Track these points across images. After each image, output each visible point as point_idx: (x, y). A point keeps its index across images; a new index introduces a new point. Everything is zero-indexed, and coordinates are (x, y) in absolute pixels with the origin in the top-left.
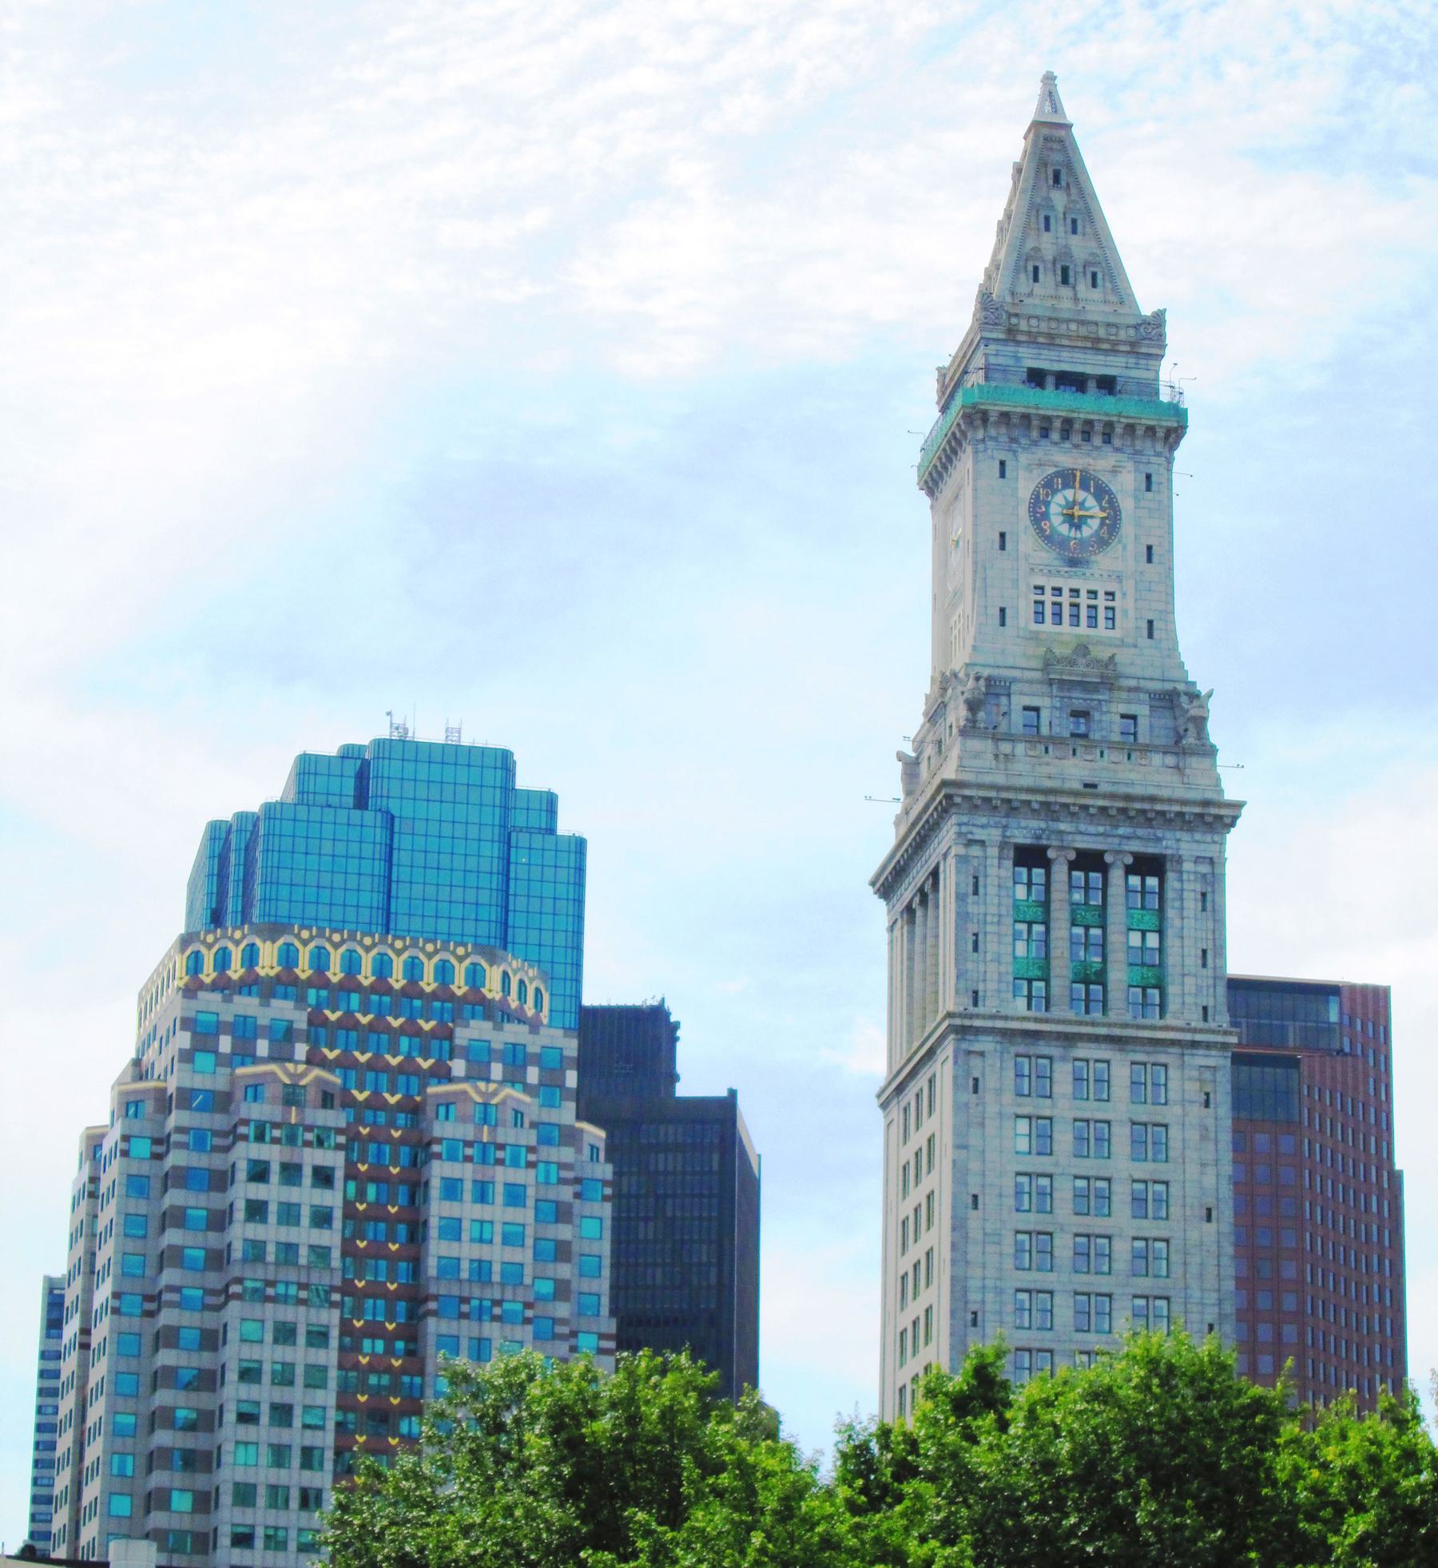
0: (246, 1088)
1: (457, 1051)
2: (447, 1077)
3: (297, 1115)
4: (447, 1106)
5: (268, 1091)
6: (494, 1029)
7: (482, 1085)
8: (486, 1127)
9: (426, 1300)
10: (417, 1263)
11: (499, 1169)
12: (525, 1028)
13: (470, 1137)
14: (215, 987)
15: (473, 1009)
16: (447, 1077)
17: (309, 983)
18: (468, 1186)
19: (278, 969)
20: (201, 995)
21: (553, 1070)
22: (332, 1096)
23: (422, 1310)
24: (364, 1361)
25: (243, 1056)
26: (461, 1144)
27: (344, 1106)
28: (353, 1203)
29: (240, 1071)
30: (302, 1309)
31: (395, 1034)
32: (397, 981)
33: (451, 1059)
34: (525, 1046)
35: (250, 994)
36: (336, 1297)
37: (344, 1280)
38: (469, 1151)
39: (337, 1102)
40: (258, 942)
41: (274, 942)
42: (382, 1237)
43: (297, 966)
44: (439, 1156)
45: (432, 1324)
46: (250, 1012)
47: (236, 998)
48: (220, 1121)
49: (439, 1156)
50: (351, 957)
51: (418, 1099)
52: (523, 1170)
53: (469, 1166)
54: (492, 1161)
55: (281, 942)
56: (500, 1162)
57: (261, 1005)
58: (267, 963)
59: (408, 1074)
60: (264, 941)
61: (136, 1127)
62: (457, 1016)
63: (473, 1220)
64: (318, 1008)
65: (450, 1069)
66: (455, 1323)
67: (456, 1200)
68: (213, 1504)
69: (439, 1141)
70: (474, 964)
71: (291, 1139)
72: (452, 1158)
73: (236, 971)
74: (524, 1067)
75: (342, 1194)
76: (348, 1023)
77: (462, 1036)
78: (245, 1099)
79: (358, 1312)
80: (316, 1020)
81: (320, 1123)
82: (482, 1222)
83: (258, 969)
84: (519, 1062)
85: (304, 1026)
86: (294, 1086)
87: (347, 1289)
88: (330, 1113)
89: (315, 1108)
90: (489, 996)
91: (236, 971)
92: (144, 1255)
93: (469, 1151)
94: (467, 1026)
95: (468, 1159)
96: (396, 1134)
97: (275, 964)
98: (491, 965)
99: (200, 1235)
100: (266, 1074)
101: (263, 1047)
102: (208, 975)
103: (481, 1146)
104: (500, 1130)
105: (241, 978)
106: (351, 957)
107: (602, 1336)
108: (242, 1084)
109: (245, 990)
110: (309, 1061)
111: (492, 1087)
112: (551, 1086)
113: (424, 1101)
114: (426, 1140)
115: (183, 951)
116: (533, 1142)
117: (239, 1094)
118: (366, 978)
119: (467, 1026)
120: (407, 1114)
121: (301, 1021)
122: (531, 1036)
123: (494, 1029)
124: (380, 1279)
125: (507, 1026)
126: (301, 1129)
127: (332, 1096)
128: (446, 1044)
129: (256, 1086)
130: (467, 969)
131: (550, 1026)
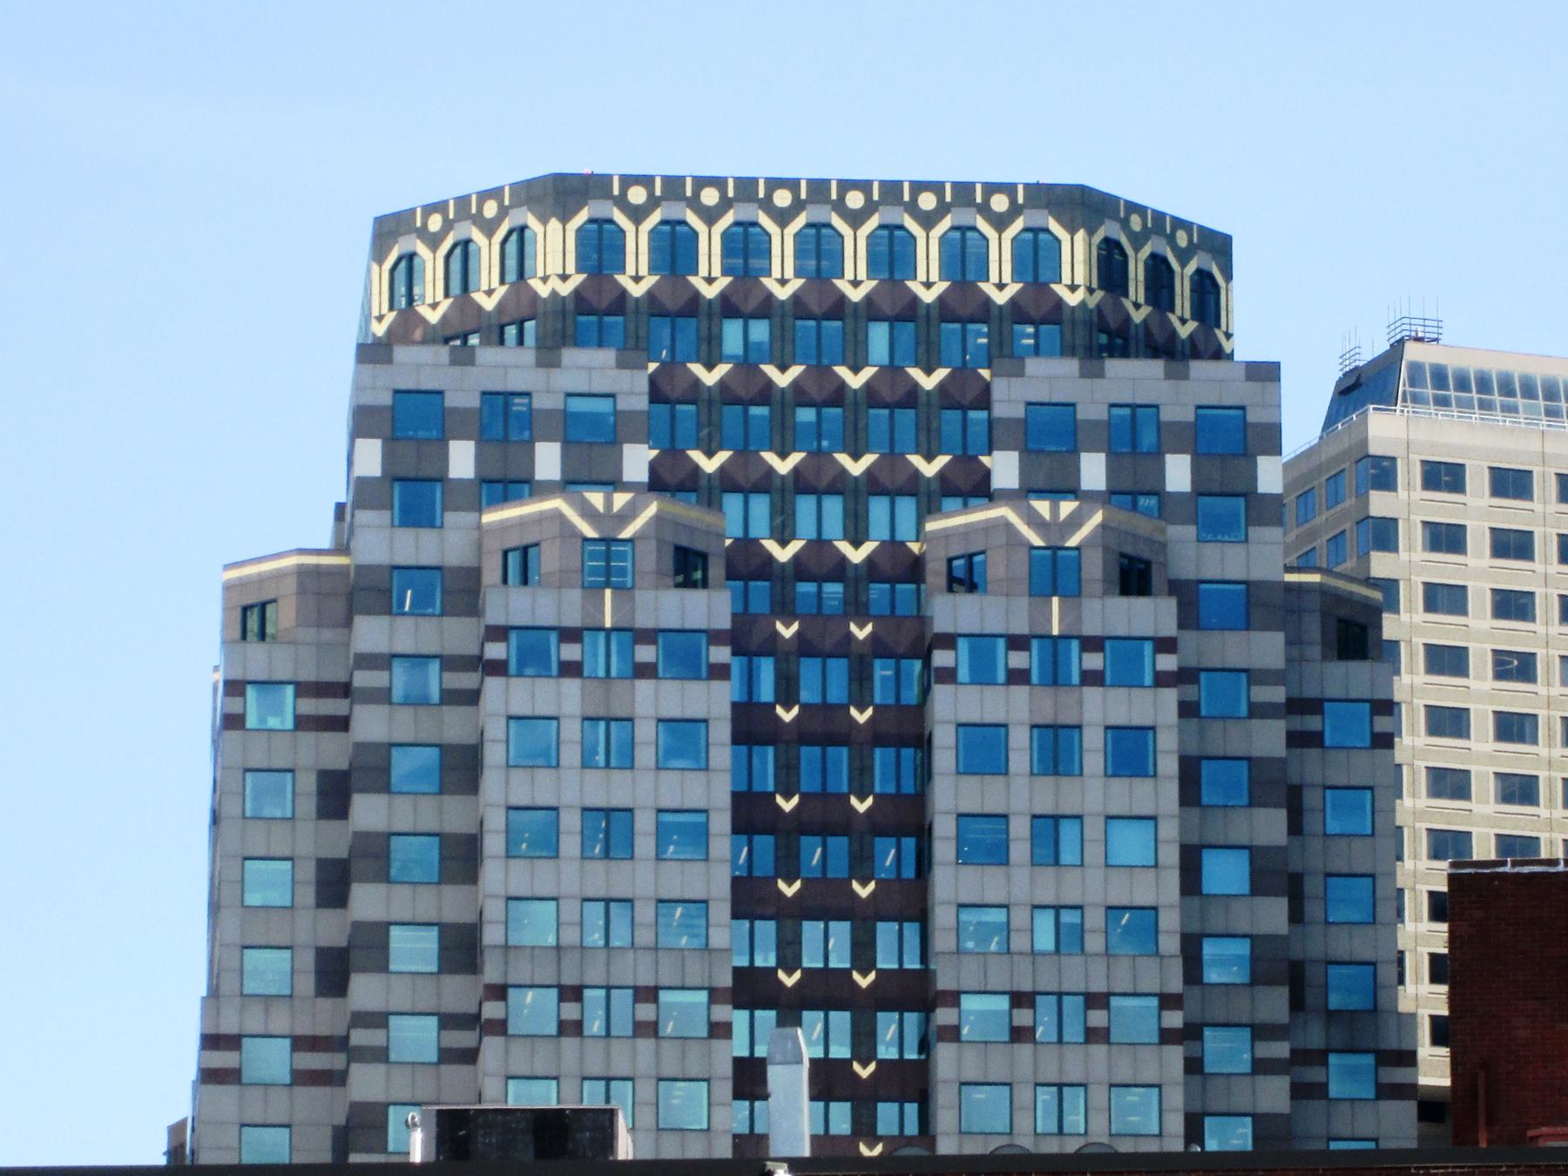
0: (505, 553)
2: (979, 488)
5: (549, 560)
7: (596, 498)
12: (1157, 367)
13: (1020, 627)
14: (444, 335)
16: (979, 488)
18: (1020, 740)
19: (577, 280)
29: (490, 518)
31: (783, 403)
38: (1018, 660)
41: (564, 220)
42: (838, 869)
43: (622, 270)
46: (515, 383)
48: (459, 635)
49: (949, 675)
51: (915, 547)
53: (1020, 693)
54: (1076, 679)
55: (582, 217)
56: (1092, 678)
57: (1084, 374)
58: (555, 267)
59: (893, 493)
60: (544, 221)
61: (258, 660)
62: (1003, 354)
65: (987, 474)
67: (1069, 774)
71: (1055, 677)
72: (982, 676)
74: (1158, 455)
77: (1009, 399)
78: (505, 581)
83: (535, 283)
84: (1148, 440)
85: (641, 403)
86: (608, 541)
88: (696, 597)
93: (1018, 660)
94: (1020, 373)
95: (1018, 677)
97: (571, 269)
99: (427, 895)
100: (541, 518)
101: (548, 460)
102: (434, 306)
107: (380, 1055)
108: (494, 547)
110: (657, 484)
111: (621, 499)
116: (1169, 627)
117: (491, 575)
118: (856, 283)
119: (1020, 373)
121: (632, 388)
122: (542, 372)
124: (759, 962)
125: (1116, 367)
126: (1075, 645)
129: (525, 550)
131: (1036, 351)
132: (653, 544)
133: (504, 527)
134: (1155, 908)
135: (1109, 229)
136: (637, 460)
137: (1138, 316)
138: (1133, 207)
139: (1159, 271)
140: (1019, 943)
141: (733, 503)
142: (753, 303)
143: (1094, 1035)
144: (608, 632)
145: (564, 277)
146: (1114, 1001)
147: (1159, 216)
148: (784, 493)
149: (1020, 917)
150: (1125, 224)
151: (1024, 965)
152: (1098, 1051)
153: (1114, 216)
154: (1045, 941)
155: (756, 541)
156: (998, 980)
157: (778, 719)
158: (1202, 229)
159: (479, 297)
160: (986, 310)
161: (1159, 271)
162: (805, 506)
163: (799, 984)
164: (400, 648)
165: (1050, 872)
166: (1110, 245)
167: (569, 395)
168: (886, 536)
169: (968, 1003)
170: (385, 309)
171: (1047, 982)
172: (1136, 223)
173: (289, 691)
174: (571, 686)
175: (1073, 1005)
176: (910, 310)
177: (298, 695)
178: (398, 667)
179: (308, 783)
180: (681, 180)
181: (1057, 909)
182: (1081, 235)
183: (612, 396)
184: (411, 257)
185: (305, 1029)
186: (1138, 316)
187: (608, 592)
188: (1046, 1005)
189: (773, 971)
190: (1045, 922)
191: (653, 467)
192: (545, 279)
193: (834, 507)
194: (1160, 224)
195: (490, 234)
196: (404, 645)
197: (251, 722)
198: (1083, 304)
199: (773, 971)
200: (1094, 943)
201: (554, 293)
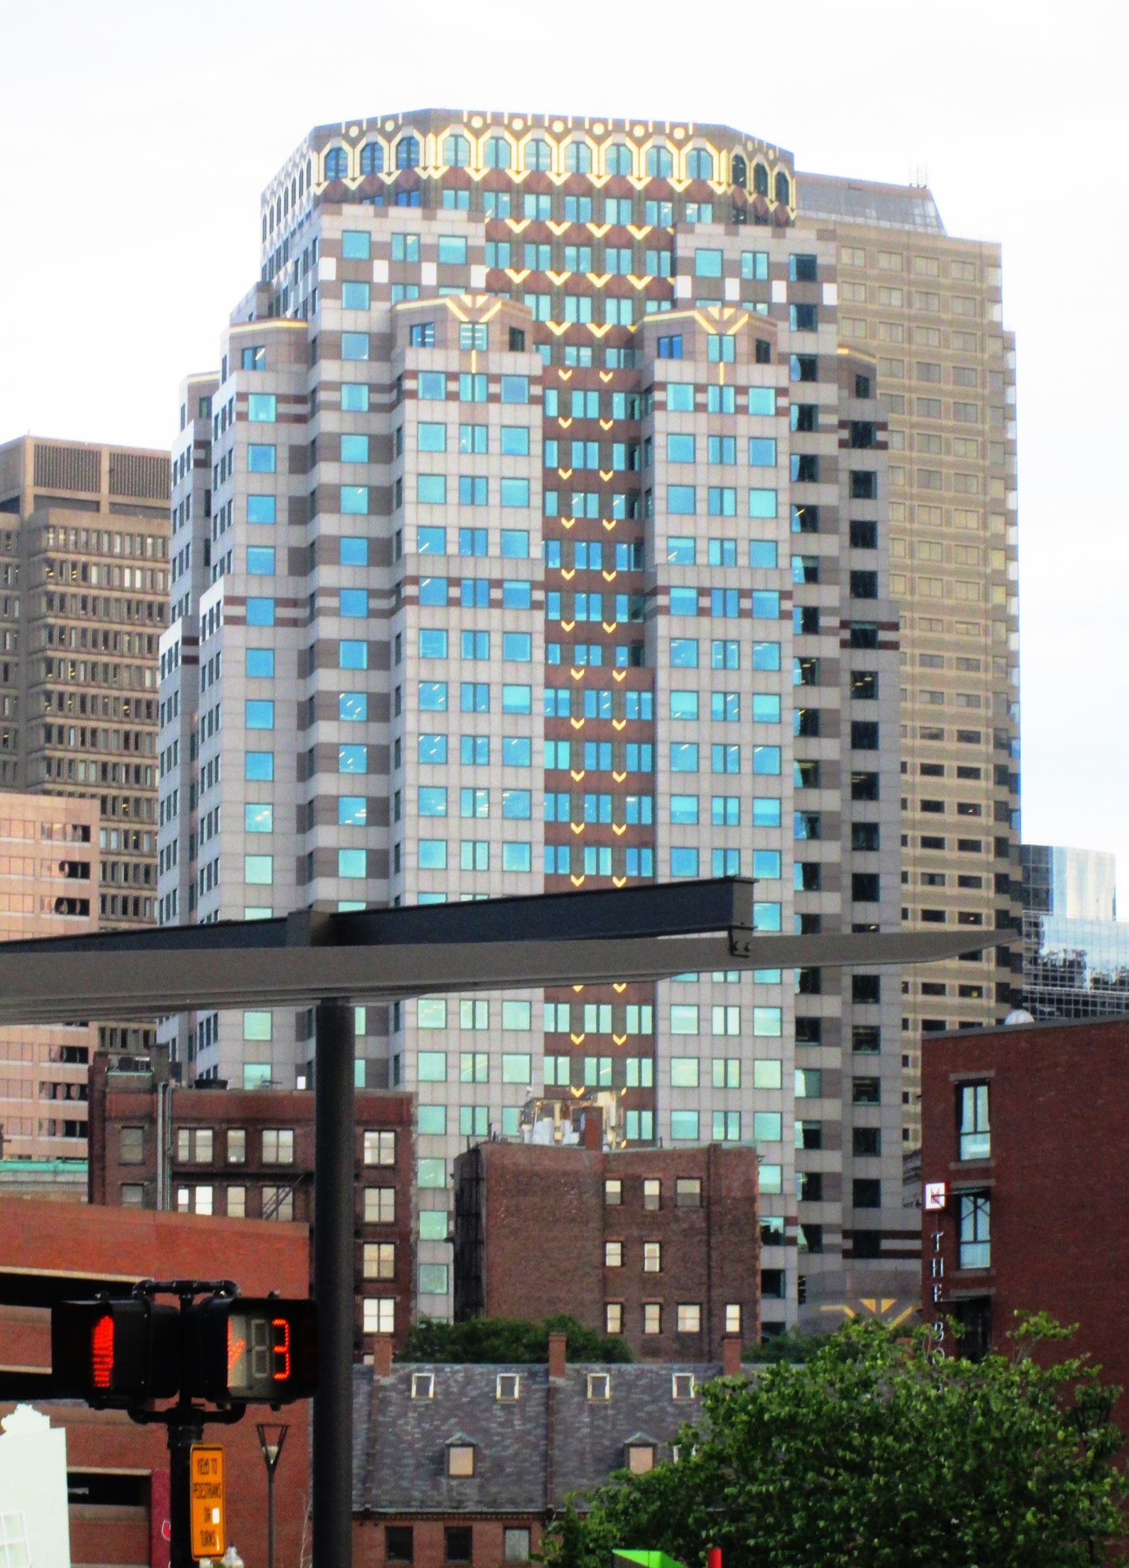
1: (679, 267)
3: (478, 363)
4: (424, 326)
6: (377, 215)
7: (714, 310)
8: (474, 353)
9: (654, 592)
10: (641, 546)
11: (493, 407)
12: (765, 232)
15: (578, 202)
17: (607, 192)
20: (347, 209)
21: (453, 267)
22: (522, 333)
23: (649, 606)
24: (578, 675)
25: (405, 285)
26: (443, 377)
27: (538, 343)
28: (555, 470)
30: (496, 612)
32: (639, 179)
33: (673, 274)
34: (369, 233)
35: (409, 204)
36: (539, 595)
37: (547, 570)
39: (528, 340)
40: (417, 135)
44: (413, 394)
45: (662, 624)
47: (394, 211)
49: (413, 394)
50: (699, 156)
51: (632, 329)
52: (692, 416)
55: (447, 133)
57: (774, 236)
63: (710, 487)
64: (496, 222)
66: (523, 615)
68: (392, 868)
69: (414, 375)
70: (699, 150)
73: (389, 174)
75: (540, 460)
76: (538, 235)
78: (411, 344)
79: (567, 611)
80: (496, 233)
81: (508, 371)
82: (473, 478)
87: (551, 583)
89: (501, 350)
90: (424, 175)
91: (389, 174)
92: (274, 547)
96: (606, 378)
97: (440, 164)
98: (424, 134)
102: (353, 179)
103: (717, 389)
104: (494, 357)
105: (396, 183)
106: (699, 156)
109: (403, 197)
110: (490, 289)
112: (356, 282)
113: (641, 331)
114: (645, 386)
115: (318, 150)
120: (619, 348)
123: (377, 215)
125: (744, 230)
126: (732, 390)
127: (522, 333)
128: (666, 255)
130: (647, 153)
132: (498, 326)
133: (412, 313)
134: (445, 528)
135: (738, 150)
136: (479, 276)
137: (751, 199)
138: (749, 138)
139: (760, 172)
140: (701, 559)
141: (530, 300)
142: (542, 186)
143: (743, 614)
144: (473, 376)
145: (436, 168)
146: (755, 594)
147: (761, 143)
148: (558, 296)
149: (702, 545)
150: (745, 146)
151: (706, 573)
152: (746, 622)
153: (740, 143)
154: (715, 558)
155: (584, 325)
156: (692, 581)
157: (601, 428)
158: (781, 150)
159: (382, 176)
160: (669, 195)
161: (760, 172)
162: (570, 302)
163: (573, 578)
164: (347, 378)
165: (718, 519)
166: (738, 159)
167: (441, 236)
168: (615, 322)
169: (675, 593)
170: (322, 179)
171: (719, 583)
172: (750, 146)
173: (273, 399)
174: (453, 406)
175: (732, 597)
176: (627, 193)
177: (278, 401)
178: (345, 389)
179: (284, 453)
180: (501, 115)
181: (722, 540)
182: (724, 153)
183: (466, 237)
184: (337, 151)
185: (282, 594)
186: (751, 199)
187: (474, 353)
188: (718, 595)
189: (600, 572)
190: (715, 547)
191: (489, 277)
192: (425, 168)
193: (586, 303)
194: (761, 147)
195: (389, 141)
196: (348, 377)
197: (251, 417)
198: (725, 193)
199: (600, 572)
200: (743, 561)
201: (430, 177)
